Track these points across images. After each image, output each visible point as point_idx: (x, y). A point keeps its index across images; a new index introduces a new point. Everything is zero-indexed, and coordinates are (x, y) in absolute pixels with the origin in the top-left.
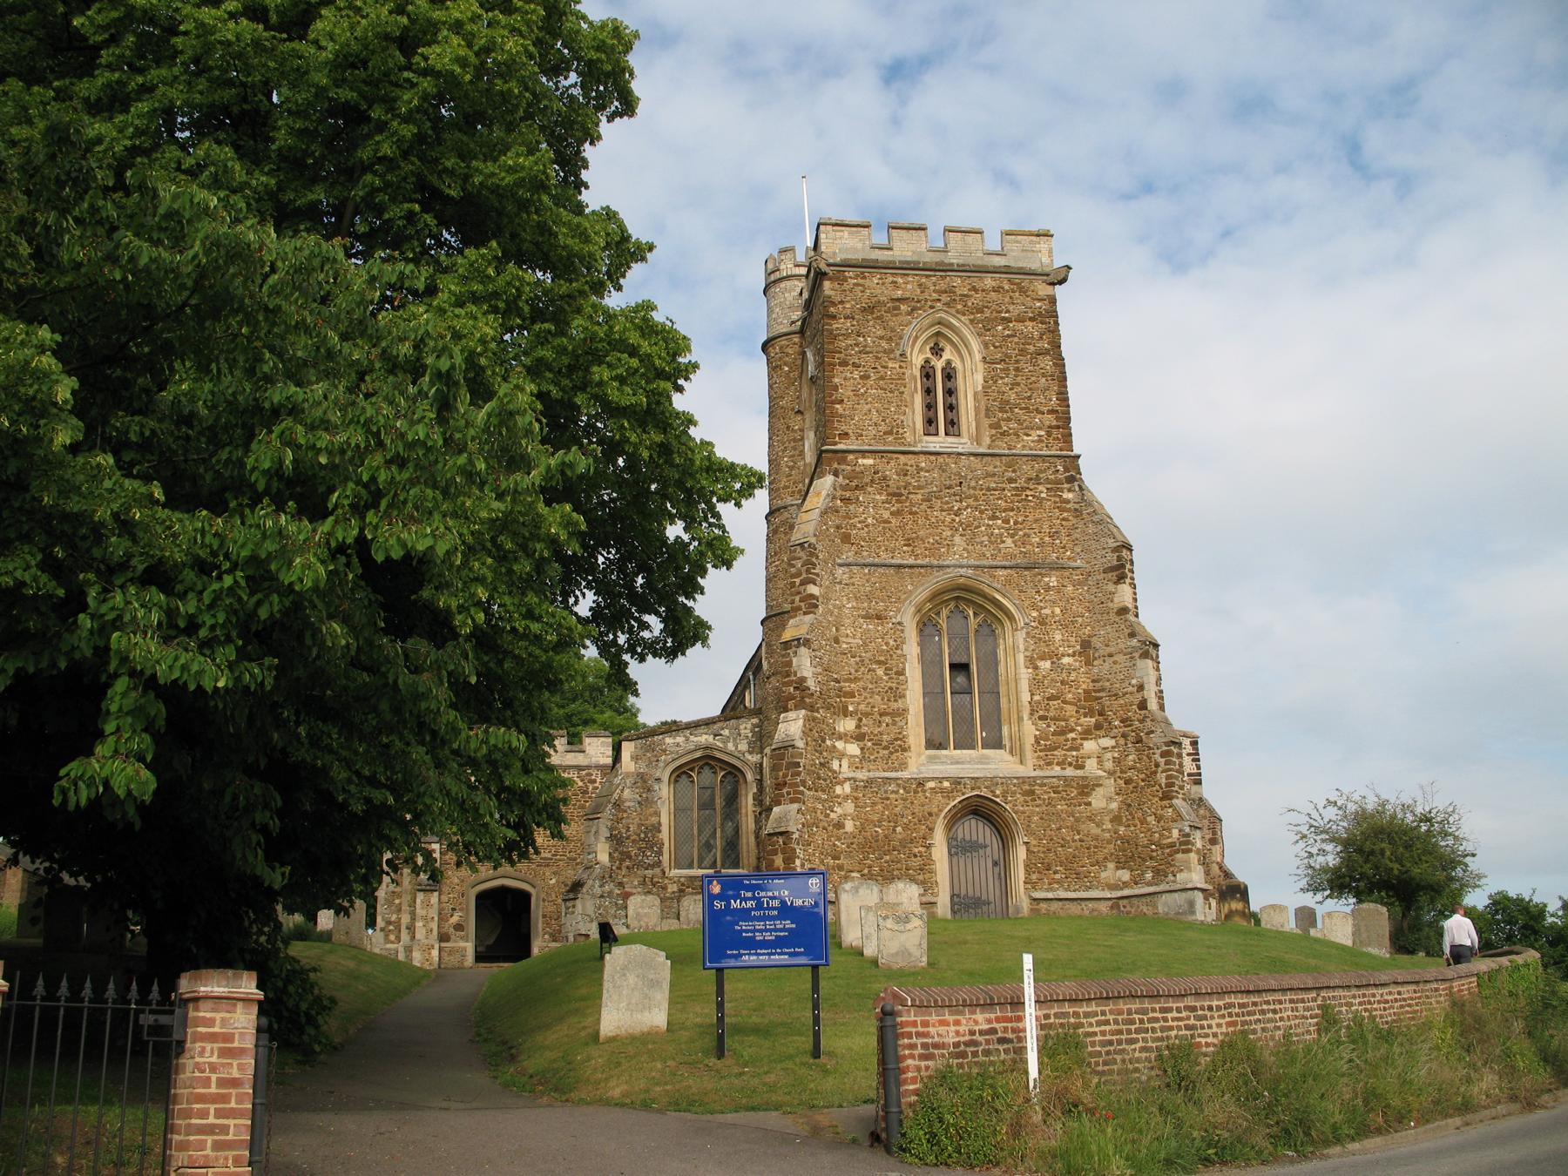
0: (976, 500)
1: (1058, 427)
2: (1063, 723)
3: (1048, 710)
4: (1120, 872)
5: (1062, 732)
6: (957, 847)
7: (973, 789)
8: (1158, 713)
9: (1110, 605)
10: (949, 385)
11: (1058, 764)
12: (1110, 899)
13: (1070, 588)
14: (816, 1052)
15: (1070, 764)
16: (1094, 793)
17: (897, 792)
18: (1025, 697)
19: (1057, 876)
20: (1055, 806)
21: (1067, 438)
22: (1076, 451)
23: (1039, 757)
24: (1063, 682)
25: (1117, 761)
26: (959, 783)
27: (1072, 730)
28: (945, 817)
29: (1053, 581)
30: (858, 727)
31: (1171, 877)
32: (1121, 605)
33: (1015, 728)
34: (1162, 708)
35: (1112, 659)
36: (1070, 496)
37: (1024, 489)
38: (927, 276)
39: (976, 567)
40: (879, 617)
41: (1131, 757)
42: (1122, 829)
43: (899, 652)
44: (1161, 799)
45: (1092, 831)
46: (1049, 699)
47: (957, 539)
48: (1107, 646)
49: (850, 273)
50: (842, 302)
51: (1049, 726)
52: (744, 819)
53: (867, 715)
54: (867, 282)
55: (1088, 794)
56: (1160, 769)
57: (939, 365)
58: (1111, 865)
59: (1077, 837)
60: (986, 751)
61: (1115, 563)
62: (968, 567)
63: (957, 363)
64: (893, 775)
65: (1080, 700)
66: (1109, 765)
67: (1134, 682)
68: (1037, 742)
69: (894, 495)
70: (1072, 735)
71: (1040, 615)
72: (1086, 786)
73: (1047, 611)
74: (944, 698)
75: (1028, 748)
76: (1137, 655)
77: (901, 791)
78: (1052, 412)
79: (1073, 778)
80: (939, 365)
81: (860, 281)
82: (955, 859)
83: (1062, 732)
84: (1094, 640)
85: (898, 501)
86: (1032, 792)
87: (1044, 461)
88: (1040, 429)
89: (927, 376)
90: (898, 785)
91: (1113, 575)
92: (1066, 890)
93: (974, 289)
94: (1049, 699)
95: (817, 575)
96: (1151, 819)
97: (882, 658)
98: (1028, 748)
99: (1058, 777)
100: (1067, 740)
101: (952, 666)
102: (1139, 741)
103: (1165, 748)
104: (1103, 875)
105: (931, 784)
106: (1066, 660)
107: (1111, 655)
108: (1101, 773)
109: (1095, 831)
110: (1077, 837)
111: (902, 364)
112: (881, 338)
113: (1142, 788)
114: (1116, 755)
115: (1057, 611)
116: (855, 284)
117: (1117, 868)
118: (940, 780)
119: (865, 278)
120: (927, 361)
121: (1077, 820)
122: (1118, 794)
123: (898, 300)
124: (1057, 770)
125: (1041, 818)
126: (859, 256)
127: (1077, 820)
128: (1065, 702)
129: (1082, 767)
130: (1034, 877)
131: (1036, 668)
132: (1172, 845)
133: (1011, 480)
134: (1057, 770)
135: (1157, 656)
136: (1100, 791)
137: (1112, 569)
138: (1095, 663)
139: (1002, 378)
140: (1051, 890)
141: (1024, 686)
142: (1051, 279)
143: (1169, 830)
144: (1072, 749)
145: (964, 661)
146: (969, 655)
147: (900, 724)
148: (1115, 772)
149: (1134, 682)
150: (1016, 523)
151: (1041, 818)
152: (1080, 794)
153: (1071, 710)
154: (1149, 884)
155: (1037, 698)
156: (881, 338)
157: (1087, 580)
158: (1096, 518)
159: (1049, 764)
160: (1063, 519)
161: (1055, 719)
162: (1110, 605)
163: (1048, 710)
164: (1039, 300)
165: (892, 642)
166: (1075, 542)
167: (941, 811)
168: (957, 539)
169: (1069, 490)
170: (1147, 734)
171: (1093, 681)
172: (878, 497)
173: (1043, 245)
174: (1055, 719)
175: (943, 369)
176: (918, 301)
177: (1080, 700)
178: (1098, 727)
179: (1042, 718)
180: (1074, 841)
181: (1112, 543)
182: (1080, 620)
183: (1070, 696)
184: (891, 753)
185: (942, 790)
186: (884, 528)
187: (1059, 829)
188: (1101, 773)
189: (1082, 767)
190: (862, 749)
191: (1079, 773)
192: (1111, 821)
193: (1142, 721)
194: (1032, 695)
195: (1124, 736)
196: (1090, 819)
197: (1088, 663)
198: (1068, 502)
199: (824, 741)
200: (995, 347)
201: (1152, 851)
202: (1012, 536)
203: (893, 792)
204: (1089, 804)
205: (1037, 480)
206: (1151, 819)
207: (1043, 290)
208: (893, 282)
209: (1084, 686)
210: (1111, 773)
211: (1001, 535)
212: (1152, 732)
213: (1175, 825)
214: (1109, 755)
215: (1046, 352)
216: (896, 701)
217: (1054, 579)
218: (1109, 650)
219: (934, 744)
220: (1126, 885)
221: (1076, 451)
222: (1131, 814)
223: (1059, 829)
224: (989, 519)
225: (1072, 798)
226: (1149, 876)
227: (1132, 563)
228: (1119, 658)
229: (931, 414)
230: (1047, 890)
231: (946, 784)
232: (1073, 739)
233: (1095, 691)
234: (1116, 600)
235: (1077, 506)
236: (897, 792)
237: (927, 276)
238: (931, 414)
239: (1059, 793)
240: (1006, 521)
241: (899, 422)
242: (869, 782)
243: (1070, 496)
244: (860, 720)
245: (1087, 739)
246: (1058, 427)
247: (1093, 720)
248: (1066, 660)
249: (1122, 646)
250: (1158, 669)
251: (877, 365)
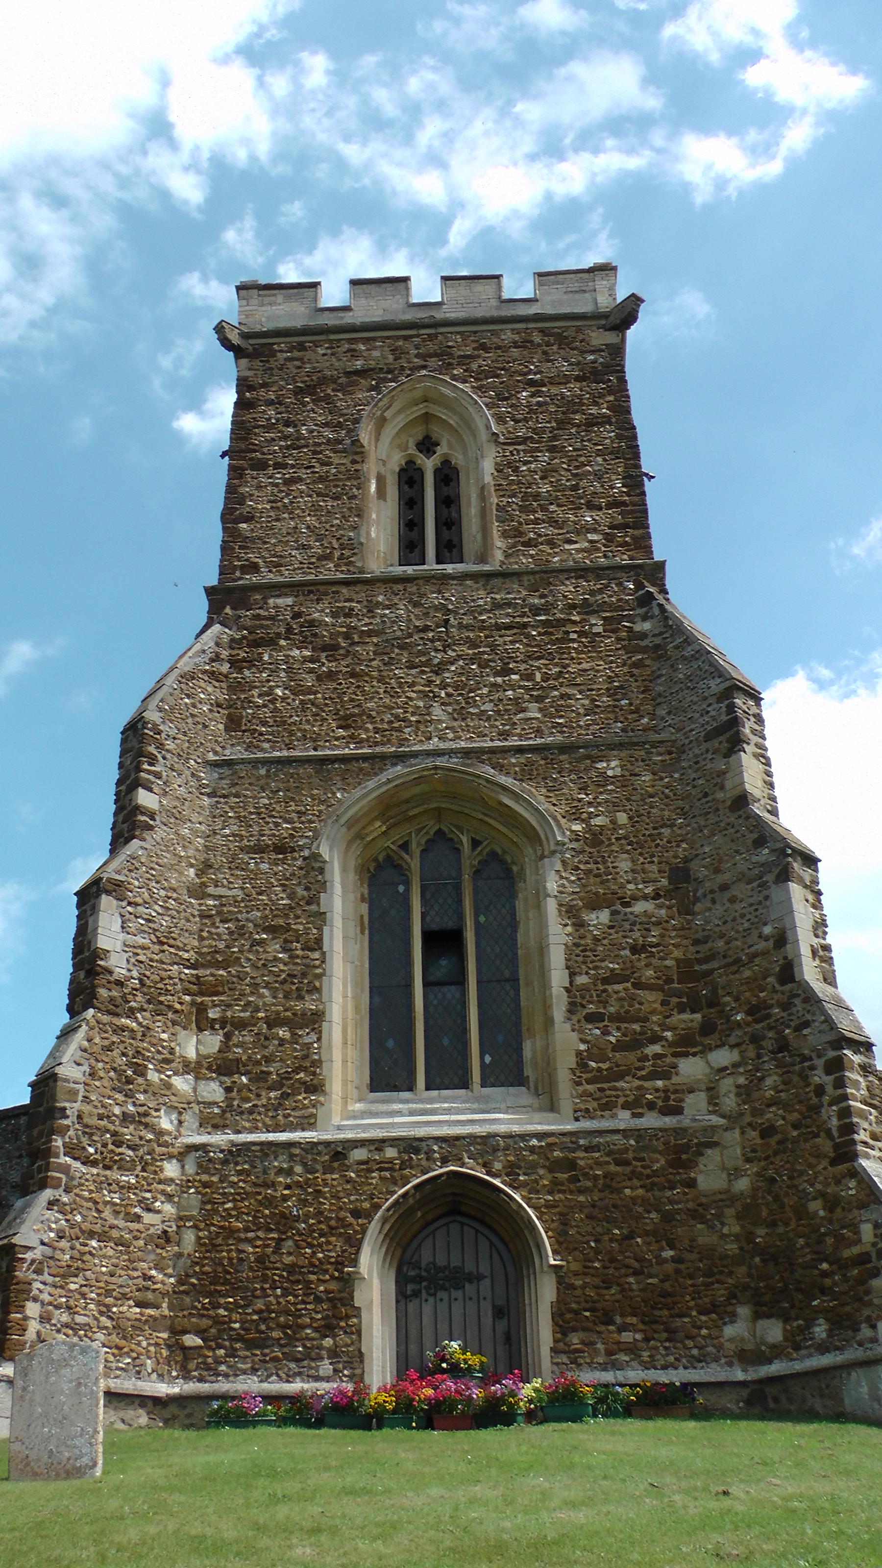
2: (636, 1027)
3: (605, 1003)
4: (763, 1324)
6: (418, 1279)
7: (445, 1161)
8: (819, 987)
9: (720, 795)
10: (445, 491)
11: (625, 1106)
13: (647, 778)
15: (651, 1106)
16: (702, 1160)
17: (289, 1172)
18: (558, 978)
19: (627, 1337)
20: (619, 1191)
21: (643, 544)
22: (658, 557)
23: (586, 1094)
26: (417, 1151)
27: (655, 1039)
28: (384, 1220)
29: (613, 767)
30: (226, 1046)
31: (866, 1332)
32: (736, 792)
34: (830, 979)
35: (727, 895)
36: (647, 626)
38: (406, 338)
39: (467, 753)
40: (280, 849)
41: (769, 1081)
42: (761, 1231)
43: (313, 907)
45: (700, 1240)
46: (606, 981)
47: (437, 712)
49: (282, 344)
50: (264, 385)
51: (605, 1033)
54: (308, 355)
55: (690, 1164)
57: (429, 465)
58: (744, 1311)
59: (668, 1253)
60: (486, 1091)
61: (724, 718)
62: (450, 752)
63: (458, 459)
65: (669, 981)
66: (730, 1103)
67: (767, 930)
69: (324, 648)
70: (656, 1048)
71: (589, 829)
72: (686, 1148)
75: (564, 1077)
76: (769, 878)
77: (298, 1169)
78: (614, 504)
81: (296, 354)
82: (412, 1306)
84: (693, 865)
85: (331, 658)
86: (572, 1165)
87: (598, 578)
88: (595, 531)
90: (292, 1156)
91: (721, 742)
92: (646, 1366)
93: (484, 347)
94: (606, 981)
95: (158, 775)
96: (816, 1207)
97: (281, 922)
98: (564, 1077)
99: (626, 1133)
100: (645, 1058)
101: (428, 937)
102: (783, 1046)
104: (729, 1331)
105: (359, 1154)
106: (639, 907)
107: (724, 887)
108: (715, 1120)
109: (705, 1237)
110: (668, 1253)
111: (357, 458)
113: (795, 1141)
114: (742, 1080)
115: (622, 818)
117: (757, 1316)
118: (379, 1144)
119: (305, 349)
120: (410, 462)
121: (668, 1218)
122: (748, 1160)
123: (357, 373)
124: (623, 1119)
125: (589, 1217)
126: (298, 323)
127: (668, 1218)
128: (637, 985)
129: (677, 1111)
130: (575, 1339)
131: (579, 925)
132: (863, 1259)
133: (536, 611)
134: (623, 1119)
135: (816, 882)
137: (719, 731)
138: (698, 907)
139: (526, 463)
140: (615, 1366)
141: (557, 958)
142: (614, 320)
143: (855, 1228)
144: (654, 1075)
145: (449, 924)
146: (461, 917)
147: (307, 1040)
148: (741, 1114)
149: (767, 930)
150: (546, 678)
151: (589, 1217)
152: (670, 1164)
153: (651, 999)
154: (823, 1348)
155: (582, 980)
156: (326, 425)
159: (608, 1107)
160: (635, 665)
161: (617, 1018)
162: (720, 795)
163: (605, 1003)
164: (593, 352)
165: (301, 892)
166: (656, 700)
167: (377, 1207)
168: (437, 712)
169: (645, 618)
170: (798, 1029)
171: (696, 942)
172: (296, 653)
174: (617, 1018)
175: (437, 472)
176: (390, 371)
178: (707, 1028)
179: (591, 1018)
180: (662, 1262)
181: (715, 686)
182: (666, 832)
183: (650, 973)
185: (384, 1166)
186: (302, 702)
187: (630, 1237)
188: (715, 1120)
189: (677, 1111)
190: (228, 1090)
191: (669, 1121)
192: (739, 1217)
193: (786, 1006)
194: (572, 975)
195: (756, 1039)
196: (696, 1215)
197: (686, 910)
198: (643, 636)
200: (517, 421)
202: (539, 699)
203: (280, 1171)
204: (692, 1184)
205: (587, 609)
207: (600, 338)
209: (677, 953)
210: (733, 1119)
211: (516, 701)
212: (807, 1024)
213: (865, 1214)
215: (605, 420)
216: (301, 998)
217: (613, 764)
218: (721, 879)
219: (427, 1089)
220: (776, 1352)
221: (658, 557)
222: (777, 1198)
223: (630, 1237)
224: (497, 674)
225: (655, 1173)
226: (820, 1330)
227: (759, 720)
229: (414, 534)
230: (604, 1368)
231: (391, 1153)
232: (657, 1056)
233: (700, 961)
234: (728, 784)
235: (658, 641)
236: (289, 1172)
237: (406, 338)
243: (647, 626)
244: (228, 1036)
245: (685, 1055)
247: (698, 1016)
248: (639, 907)
249: (742, 866)
250: (817, 905)
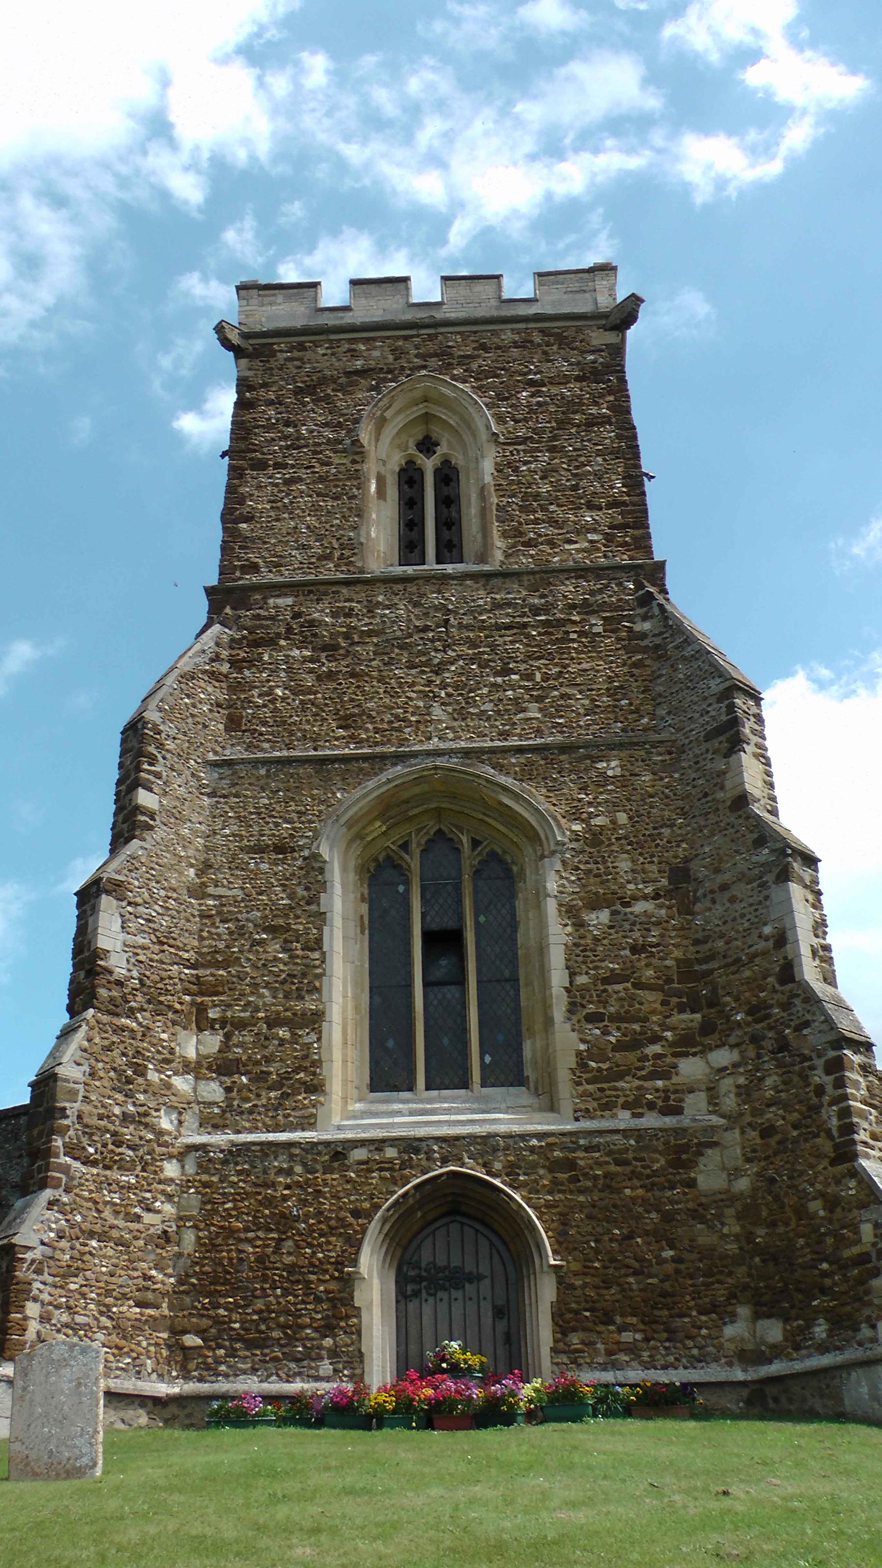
0: (473, 645)
1: (623, 527)
2: (636, 1027)
3: (605, 1003)
4: (762, 1324)
5: (632, 1044)
7: (445, 1161)
9: (720, 795)
10: (446, 491)
11: (625, 1106)
12: (743, 1384)
13: (647, 778)
14: (718, 1555)
15: (651, 1106)
16: (702, 1160)
17: (289, 1172)
18: (558, 978)
19: (627, 1337)
20: (619, 1191)
21: (643, 544)
22: (657, 557)
24: (634, 949)
25: (744, 1093)
27: (655, 1039)
28: (384, 1220)
31: (866, 1332)
33: (539, 1043)
34: (830, 979)
35: (727, 895)
36: (647, 626)
37: (561, 623)
38: (406, 338)
39: (467, 753)
40: (280, 849)
41: (769, 1082)
42: (761, 1231)
43: (313, 907)
44: (834, 1162)
45: (701, 1240)
46: (606, 981)
48: (717, 871)
49: (281, 344)
51: (605, 1033)
52: (527, 1309)
53: (241, 1025)
55: (690, 1164)
56: (826, 1099)
57: (429, 465)
58: (744, 1311)
61: (724, 718)
64: (283, 1137)
66: (730, 1102)
67: (767, 930)
68: (582, 1064)
69: (324, 648)
70: (656, 1048)
71: (589, 829)
72: (684, 1149)
73: (598, 821)
74: (410, 996)
75: (564, 1076)
77: (298, 1169)
78: (614, 504)
79: (655, 1133)
80: (429, 465)
81: (296, 354)
82: (412, 1306)
83: (632, 1044)
84: (693, 865)
87: (598, 578)
88: (595, 531)
89: (411, 482)
92: (646, 1366)
93: (484, 347)
94: (606, 981)
95: (158, 775)
96: (816, 1207)
98: (564, 1076)
99: (626, 1133)
101: (428, 937)
102: (783, 1046)
103: (832, 1054)
104: (729, 1331)
105: (359, 1154)
106: (639, 907)
107: (724, 887)
108: (715, 1120)
111: (357, 458)
112: (326, 425)
113: (795, 1141)
114: (742, 1080)
115: (622, 818)
116: (288, 359)
117: (757, 1316)
118: (379, 1144)
120: (410, 462)
121: (668, 1218)
122: (748, 1160)
123: (357, 372)
124: (623, 1119)
125: (589, 1217)
126: (299, 323)
127: (668, 1218)
128: (637, 985)
129: (678, 1111)
130: (575, 1339)
131: (580, 925)
132: (863, 1259)
134: (623, 1119)
136: (712, 1157)
137: (719, 731)
139: (526, 463)
140: (615, 1366)
141: (557, 957)
143: (855, 1228)
144: (654, 1075)
145: (450, 923)
146: (461, 917)
149: (767, 930)
151: (589, 1217)
152: (671, 1164)
153: (652, 999)
154: (823, 1348)
155: (582, 980)
157: (678, 760)
158: (688, 652)
159: (608, 1106)
161: (617, 1018)
162: (720, 795)
164: (593, 352)
165: (301, 892)
166: (656, 700)
167: (377, 1207)
168: (437, 712)
169: (645, 618)
170: (798, 1029)
171: (696, 942)
172: (296, 653)
173: (601, 284)
174: (617, 1018)
175: (437, 472)
176: (390, 371)
177: (669, 981)
178: (707, 1028)
179: (591, 1018)
182: (666, 832)
183: (650, 973)
184: (285, 1096)
185: (384, 1166)
187: (630, 1237)
188: (715, 1120)
189: (678, 1111)
190: (228, 1090)
191: (669, 1121)
192: (739, 1217)
193: (786, 1006)
194: (572, 975)
195: (755, 1039)
197: (686, 910)
198: (643, 636)
199: (141, 1072)
200: (517, 421)
201: (825, 1274)
202: (539, 699)
203: (280, 1171)
204: (692, 1184)
206: (816, 1207)
207: (600, 338)
208: (349, 350)
209: (677, 953)
210: (733, 1119)
212: (807, 1024)
213: (865, 1214)
214: (727, 1084)
216: (301, 998)
217: (613, 764)
218: (720, 879)
219: (427, 1089)
220: (775, 1352)
221: (657, 557)
222: (777, 1198)
223: (630, 1237)
224: (497, 674)
225: (655, 1173)
226: (820, 1330)
227: (759, 720)
228: (740, 890)
229: (414, 535)
230: (604, 1367)
231: (391, 1153)
232: (657, 1056)
233: (699, 962)
234: (728, 784)
235: (658, 640)
236: (289, 1172)
237: (406, 338)
238: (414, 535)
239: (625, 1163)
240: (529, 677)
241: (345, 540)
242: (237, 1152)
244: (228, 1036)
245: (685, 1055)
246: (623, 527)
247: (698, 1016)
248: (639, 907)
249: (743, 867)
250: (817, 905)
251: (314, 462)
